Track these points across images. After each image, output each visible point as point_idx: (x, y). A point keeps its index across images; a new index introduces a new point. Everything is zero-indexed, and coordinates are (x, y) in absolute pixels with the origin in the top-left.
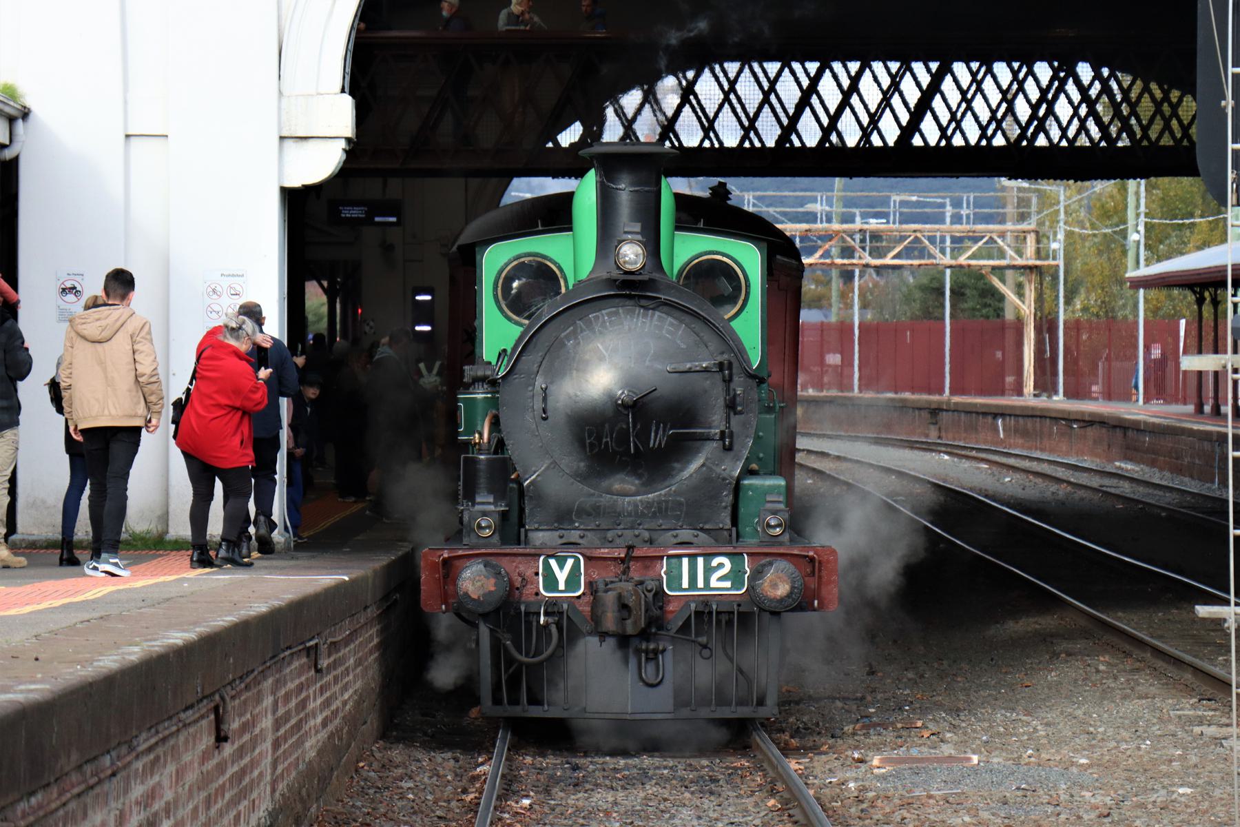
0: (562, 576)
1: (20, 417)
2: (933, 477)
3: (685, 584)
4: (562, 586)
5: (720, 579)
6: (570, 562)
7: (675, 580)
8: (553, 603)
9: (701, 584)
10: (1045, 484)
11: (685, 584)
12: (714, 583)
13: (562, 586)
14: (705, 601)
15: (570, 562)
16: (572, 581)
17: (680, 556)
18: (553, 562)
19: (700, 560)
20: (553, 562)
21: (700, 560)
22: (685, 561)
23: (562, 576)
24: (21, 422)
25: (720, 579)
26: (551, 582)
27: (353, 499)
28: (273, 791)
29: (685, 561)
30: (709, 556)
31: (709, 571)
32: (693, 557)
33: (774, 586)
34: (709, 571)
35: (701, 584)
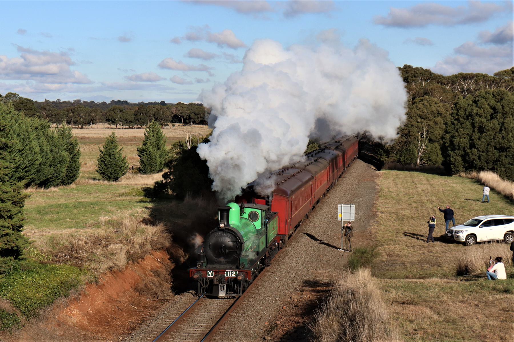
0: (210, 274)
1: (89, 101)
2: (198, 100)
3: (228, 275)
4: (210, 275)
5: (234, 275)
6: (211, 272)
7: (227, 275)
8: (209, 277)
9: (231, 275)
10: (23, 217)
11: (228, 275)
12: (233, 275)
13: (210, 275)
14: (231, 278)
15: (211, 272)
16: (212, 275)
17: (228, 271)
18: (209, 272)
19: (231, 272)
20: (209, 272)
21: (231, 272)
22: (228, 272)
23: (210, 274)
24: (126, 100)
25: (234, 275)
26: (209, 275)
27: (374, 168)
28: (407, 261)
29: (228, 272)
30: (232, 272)
31: (232, 274)
32: (230, 272)
33: (239, 278)
34: (232, 274)
35: (231, 275)
